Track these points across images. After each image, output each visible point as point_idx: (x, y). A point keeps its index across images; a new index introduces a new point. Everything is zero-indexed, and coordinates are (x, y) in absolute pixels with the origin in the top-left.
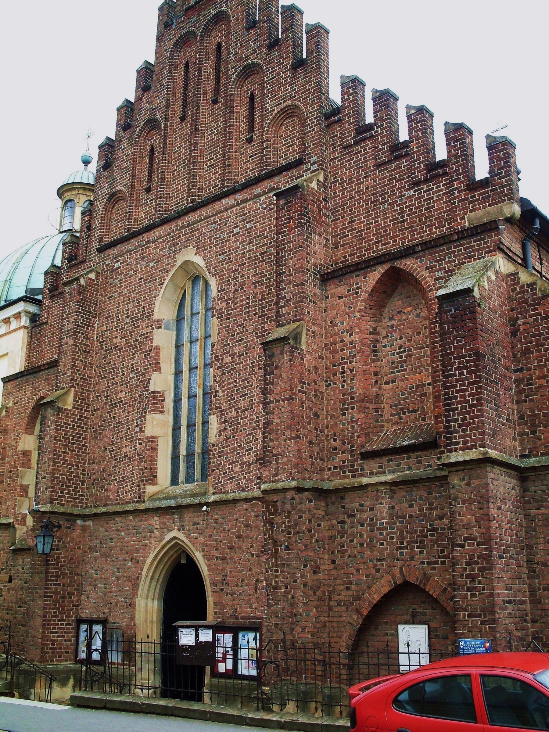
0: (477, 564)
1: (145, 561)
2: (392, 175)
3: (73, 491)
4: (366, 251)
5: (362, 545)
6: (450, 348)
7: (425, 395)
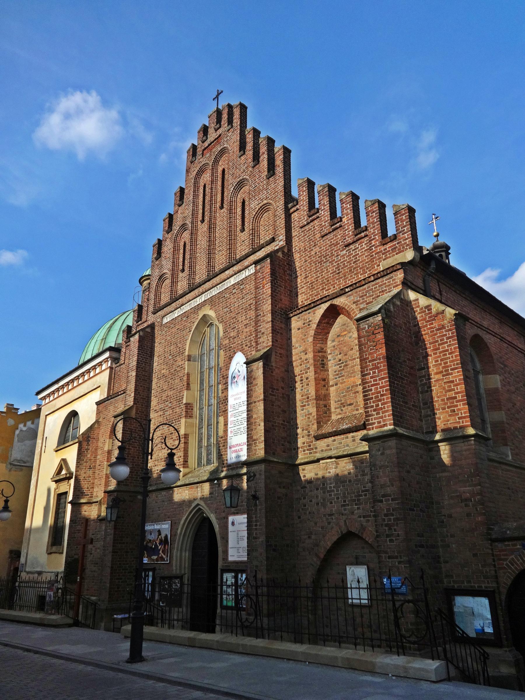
0: (393, 515)
1: (180, 523)
2: (331, 242)
3: (135, 475)
5: (318, 504)
7: (358, 392)
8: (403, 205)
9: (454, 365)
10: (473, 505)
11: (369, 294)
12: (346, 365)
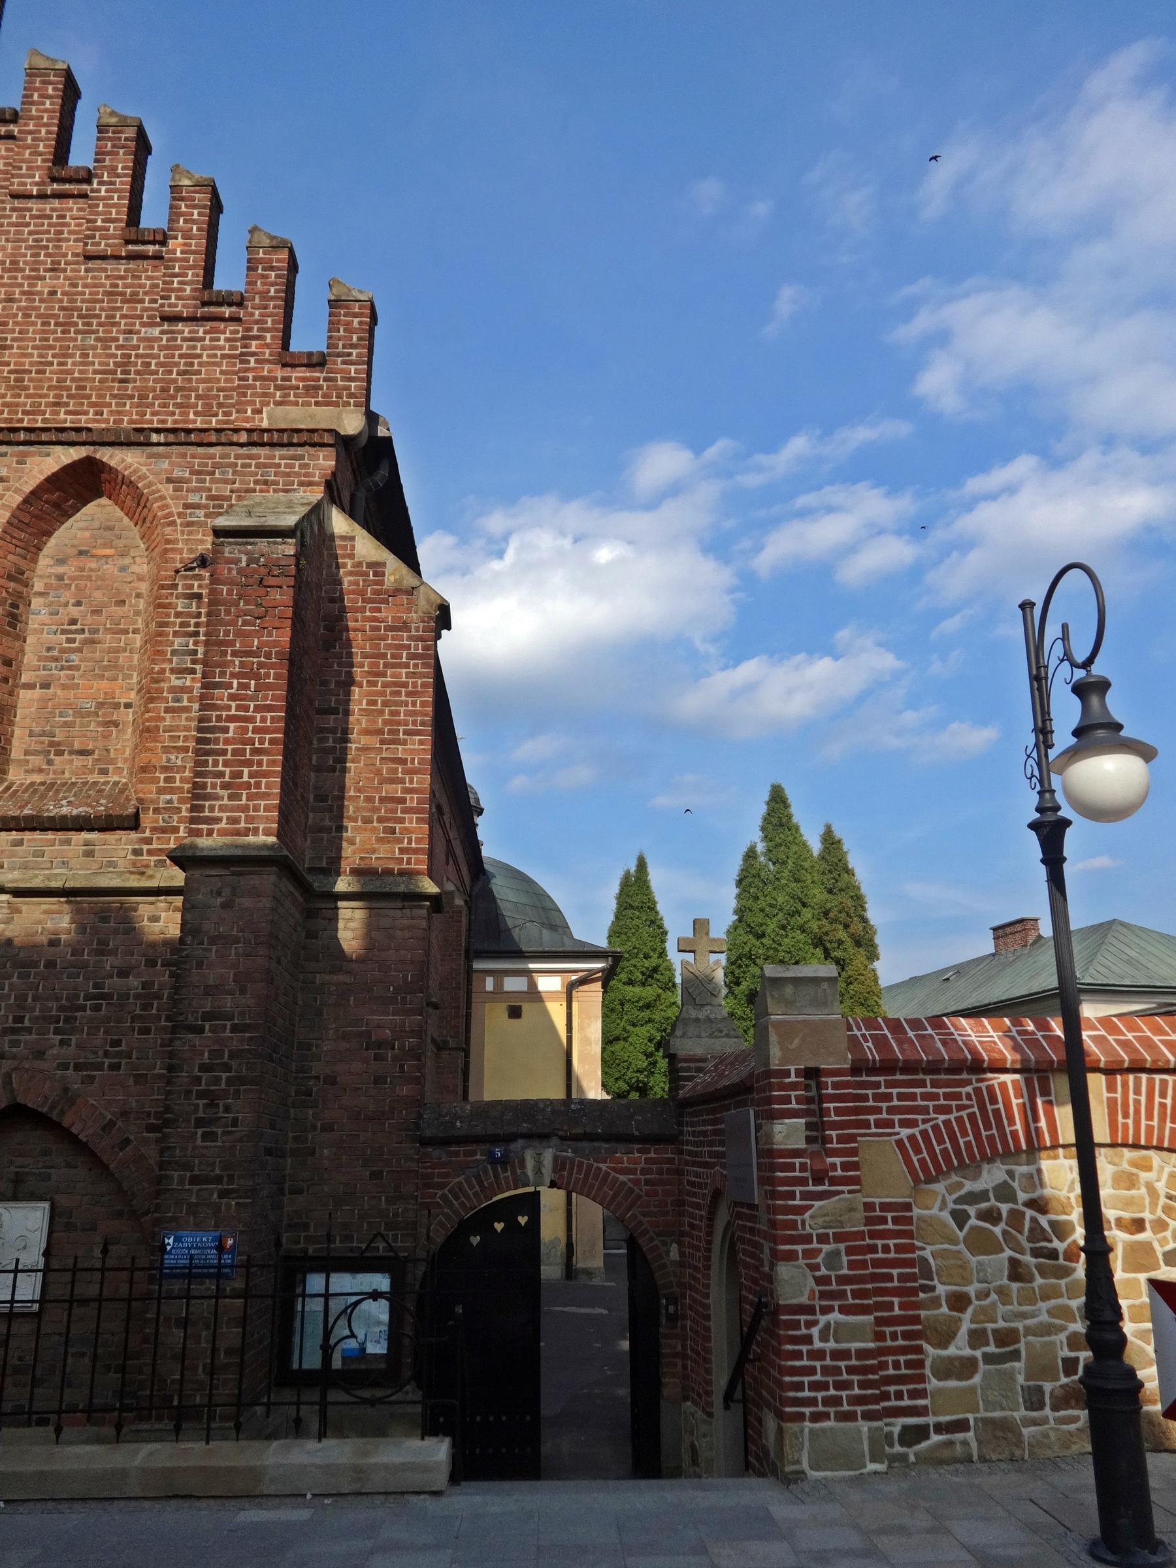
0: (227, 1068)
2: (117, 286)
4: (25, 413)
6: (227, 633)
7: (116, 724)
8: (361, 292)
9: (414, 723)
10: (395, 1058)
11: (223, 473)
12: (93, 642)
